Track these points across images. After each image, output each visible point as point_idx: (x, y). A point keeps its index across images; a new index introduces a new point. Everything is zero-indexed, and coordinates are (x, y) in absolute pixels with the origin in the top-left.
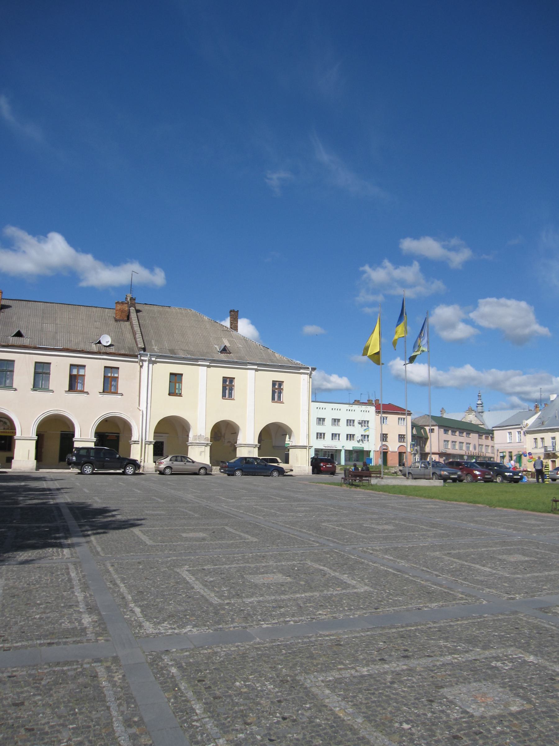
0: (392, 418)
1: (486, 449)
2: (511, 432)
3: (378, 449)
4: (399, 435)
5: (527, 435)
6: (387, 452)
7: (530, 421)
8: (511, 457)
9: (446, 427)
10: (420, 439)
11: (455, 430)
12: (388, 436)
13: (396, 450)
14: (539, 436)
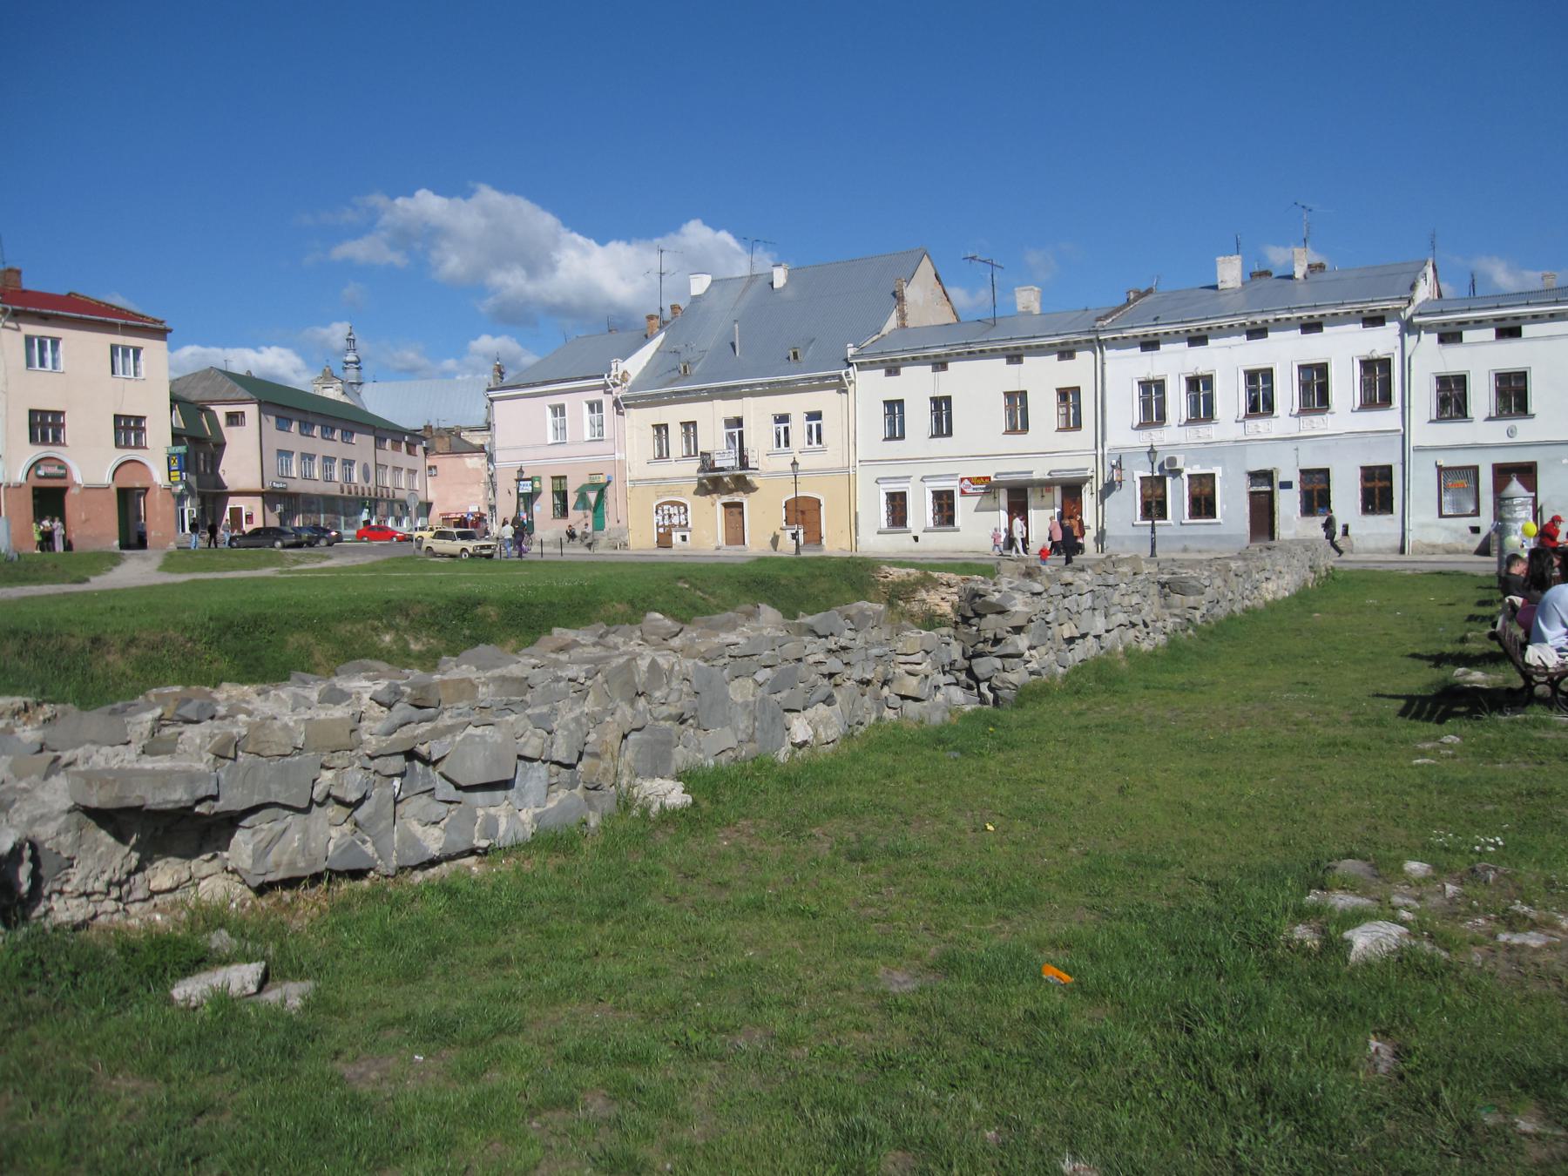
0: (83, 349)
1: (394, 479)
2: (562, 407)
3: (19, 477)
4: (117, 418)
5: (627, 411)
6: (63, 490)
8: (562, 495)
9: (284, 407)
10: (198, 448)
11: (311, 419)
12: (68, 420)
13: (107, 479)
14: (673, 415)
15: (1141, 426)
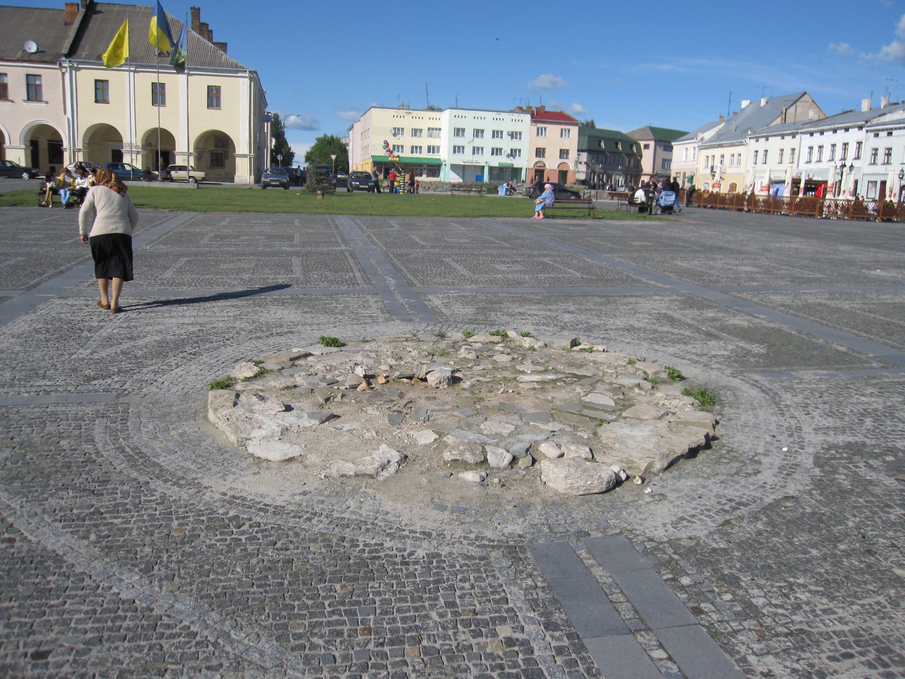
0: (553, 130)
3: (532, 166)
7: (708, 135)
8: (684, 177)
15: (807, 163)
